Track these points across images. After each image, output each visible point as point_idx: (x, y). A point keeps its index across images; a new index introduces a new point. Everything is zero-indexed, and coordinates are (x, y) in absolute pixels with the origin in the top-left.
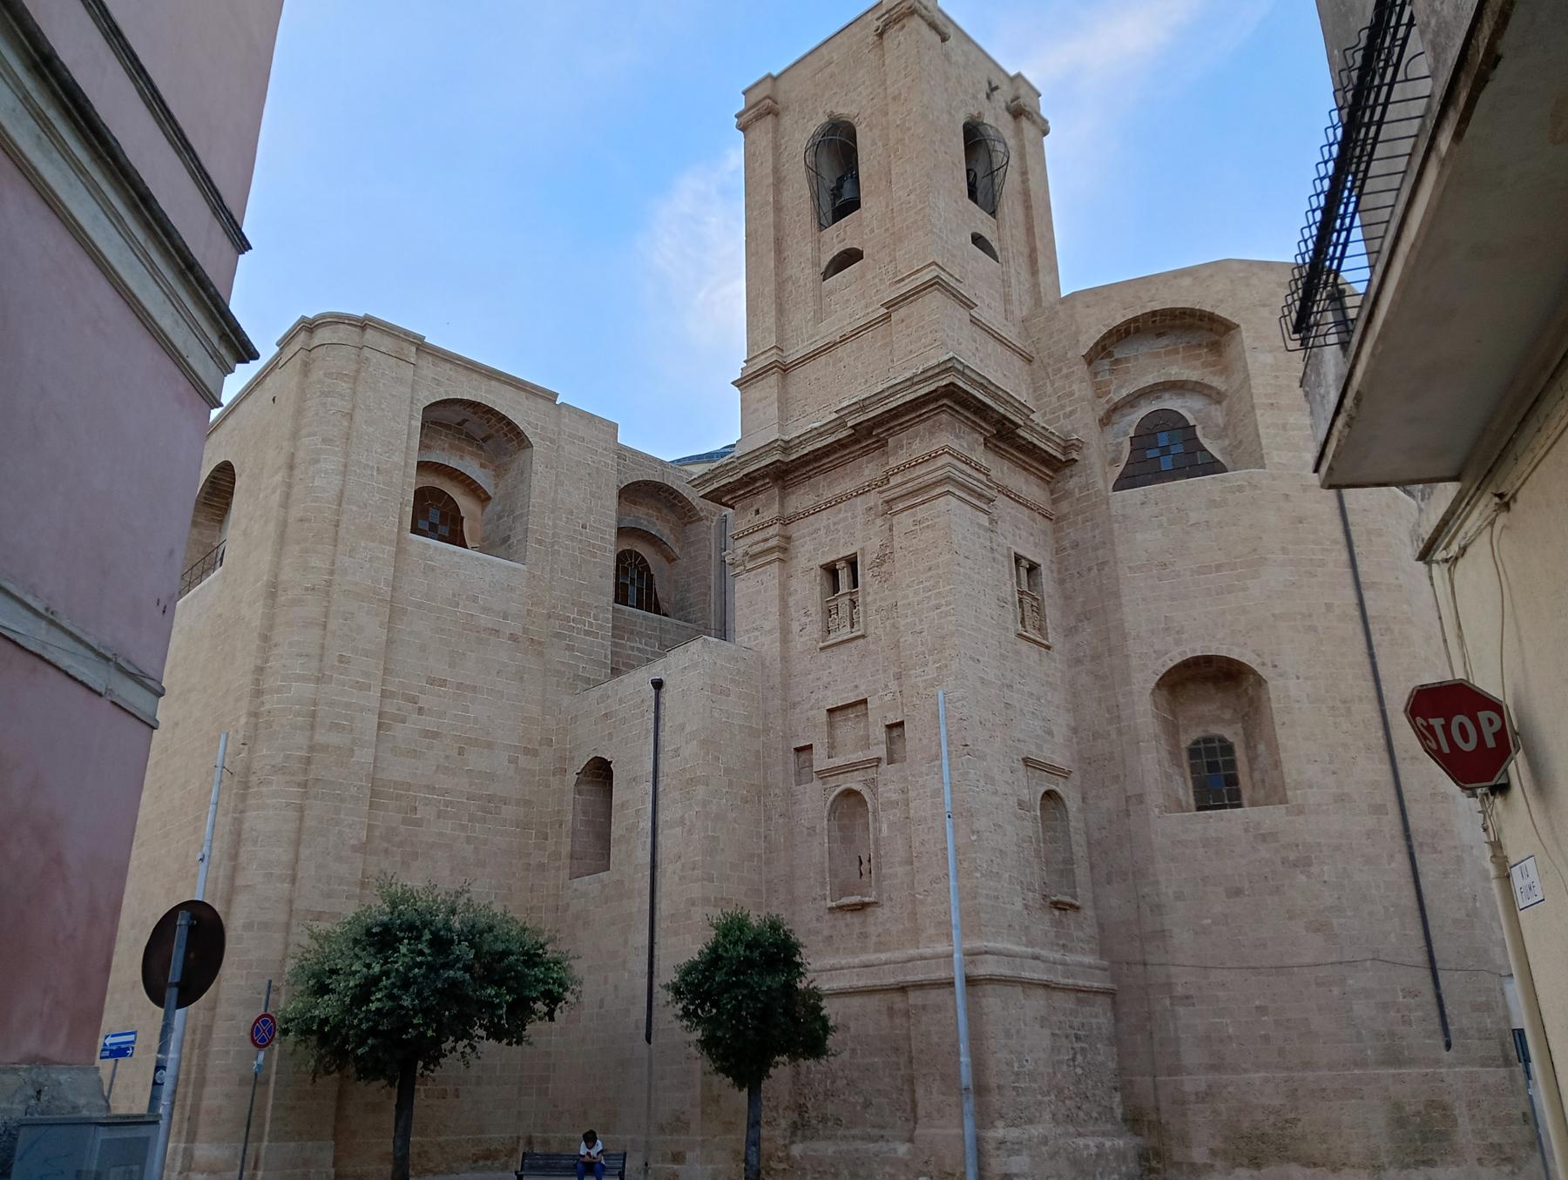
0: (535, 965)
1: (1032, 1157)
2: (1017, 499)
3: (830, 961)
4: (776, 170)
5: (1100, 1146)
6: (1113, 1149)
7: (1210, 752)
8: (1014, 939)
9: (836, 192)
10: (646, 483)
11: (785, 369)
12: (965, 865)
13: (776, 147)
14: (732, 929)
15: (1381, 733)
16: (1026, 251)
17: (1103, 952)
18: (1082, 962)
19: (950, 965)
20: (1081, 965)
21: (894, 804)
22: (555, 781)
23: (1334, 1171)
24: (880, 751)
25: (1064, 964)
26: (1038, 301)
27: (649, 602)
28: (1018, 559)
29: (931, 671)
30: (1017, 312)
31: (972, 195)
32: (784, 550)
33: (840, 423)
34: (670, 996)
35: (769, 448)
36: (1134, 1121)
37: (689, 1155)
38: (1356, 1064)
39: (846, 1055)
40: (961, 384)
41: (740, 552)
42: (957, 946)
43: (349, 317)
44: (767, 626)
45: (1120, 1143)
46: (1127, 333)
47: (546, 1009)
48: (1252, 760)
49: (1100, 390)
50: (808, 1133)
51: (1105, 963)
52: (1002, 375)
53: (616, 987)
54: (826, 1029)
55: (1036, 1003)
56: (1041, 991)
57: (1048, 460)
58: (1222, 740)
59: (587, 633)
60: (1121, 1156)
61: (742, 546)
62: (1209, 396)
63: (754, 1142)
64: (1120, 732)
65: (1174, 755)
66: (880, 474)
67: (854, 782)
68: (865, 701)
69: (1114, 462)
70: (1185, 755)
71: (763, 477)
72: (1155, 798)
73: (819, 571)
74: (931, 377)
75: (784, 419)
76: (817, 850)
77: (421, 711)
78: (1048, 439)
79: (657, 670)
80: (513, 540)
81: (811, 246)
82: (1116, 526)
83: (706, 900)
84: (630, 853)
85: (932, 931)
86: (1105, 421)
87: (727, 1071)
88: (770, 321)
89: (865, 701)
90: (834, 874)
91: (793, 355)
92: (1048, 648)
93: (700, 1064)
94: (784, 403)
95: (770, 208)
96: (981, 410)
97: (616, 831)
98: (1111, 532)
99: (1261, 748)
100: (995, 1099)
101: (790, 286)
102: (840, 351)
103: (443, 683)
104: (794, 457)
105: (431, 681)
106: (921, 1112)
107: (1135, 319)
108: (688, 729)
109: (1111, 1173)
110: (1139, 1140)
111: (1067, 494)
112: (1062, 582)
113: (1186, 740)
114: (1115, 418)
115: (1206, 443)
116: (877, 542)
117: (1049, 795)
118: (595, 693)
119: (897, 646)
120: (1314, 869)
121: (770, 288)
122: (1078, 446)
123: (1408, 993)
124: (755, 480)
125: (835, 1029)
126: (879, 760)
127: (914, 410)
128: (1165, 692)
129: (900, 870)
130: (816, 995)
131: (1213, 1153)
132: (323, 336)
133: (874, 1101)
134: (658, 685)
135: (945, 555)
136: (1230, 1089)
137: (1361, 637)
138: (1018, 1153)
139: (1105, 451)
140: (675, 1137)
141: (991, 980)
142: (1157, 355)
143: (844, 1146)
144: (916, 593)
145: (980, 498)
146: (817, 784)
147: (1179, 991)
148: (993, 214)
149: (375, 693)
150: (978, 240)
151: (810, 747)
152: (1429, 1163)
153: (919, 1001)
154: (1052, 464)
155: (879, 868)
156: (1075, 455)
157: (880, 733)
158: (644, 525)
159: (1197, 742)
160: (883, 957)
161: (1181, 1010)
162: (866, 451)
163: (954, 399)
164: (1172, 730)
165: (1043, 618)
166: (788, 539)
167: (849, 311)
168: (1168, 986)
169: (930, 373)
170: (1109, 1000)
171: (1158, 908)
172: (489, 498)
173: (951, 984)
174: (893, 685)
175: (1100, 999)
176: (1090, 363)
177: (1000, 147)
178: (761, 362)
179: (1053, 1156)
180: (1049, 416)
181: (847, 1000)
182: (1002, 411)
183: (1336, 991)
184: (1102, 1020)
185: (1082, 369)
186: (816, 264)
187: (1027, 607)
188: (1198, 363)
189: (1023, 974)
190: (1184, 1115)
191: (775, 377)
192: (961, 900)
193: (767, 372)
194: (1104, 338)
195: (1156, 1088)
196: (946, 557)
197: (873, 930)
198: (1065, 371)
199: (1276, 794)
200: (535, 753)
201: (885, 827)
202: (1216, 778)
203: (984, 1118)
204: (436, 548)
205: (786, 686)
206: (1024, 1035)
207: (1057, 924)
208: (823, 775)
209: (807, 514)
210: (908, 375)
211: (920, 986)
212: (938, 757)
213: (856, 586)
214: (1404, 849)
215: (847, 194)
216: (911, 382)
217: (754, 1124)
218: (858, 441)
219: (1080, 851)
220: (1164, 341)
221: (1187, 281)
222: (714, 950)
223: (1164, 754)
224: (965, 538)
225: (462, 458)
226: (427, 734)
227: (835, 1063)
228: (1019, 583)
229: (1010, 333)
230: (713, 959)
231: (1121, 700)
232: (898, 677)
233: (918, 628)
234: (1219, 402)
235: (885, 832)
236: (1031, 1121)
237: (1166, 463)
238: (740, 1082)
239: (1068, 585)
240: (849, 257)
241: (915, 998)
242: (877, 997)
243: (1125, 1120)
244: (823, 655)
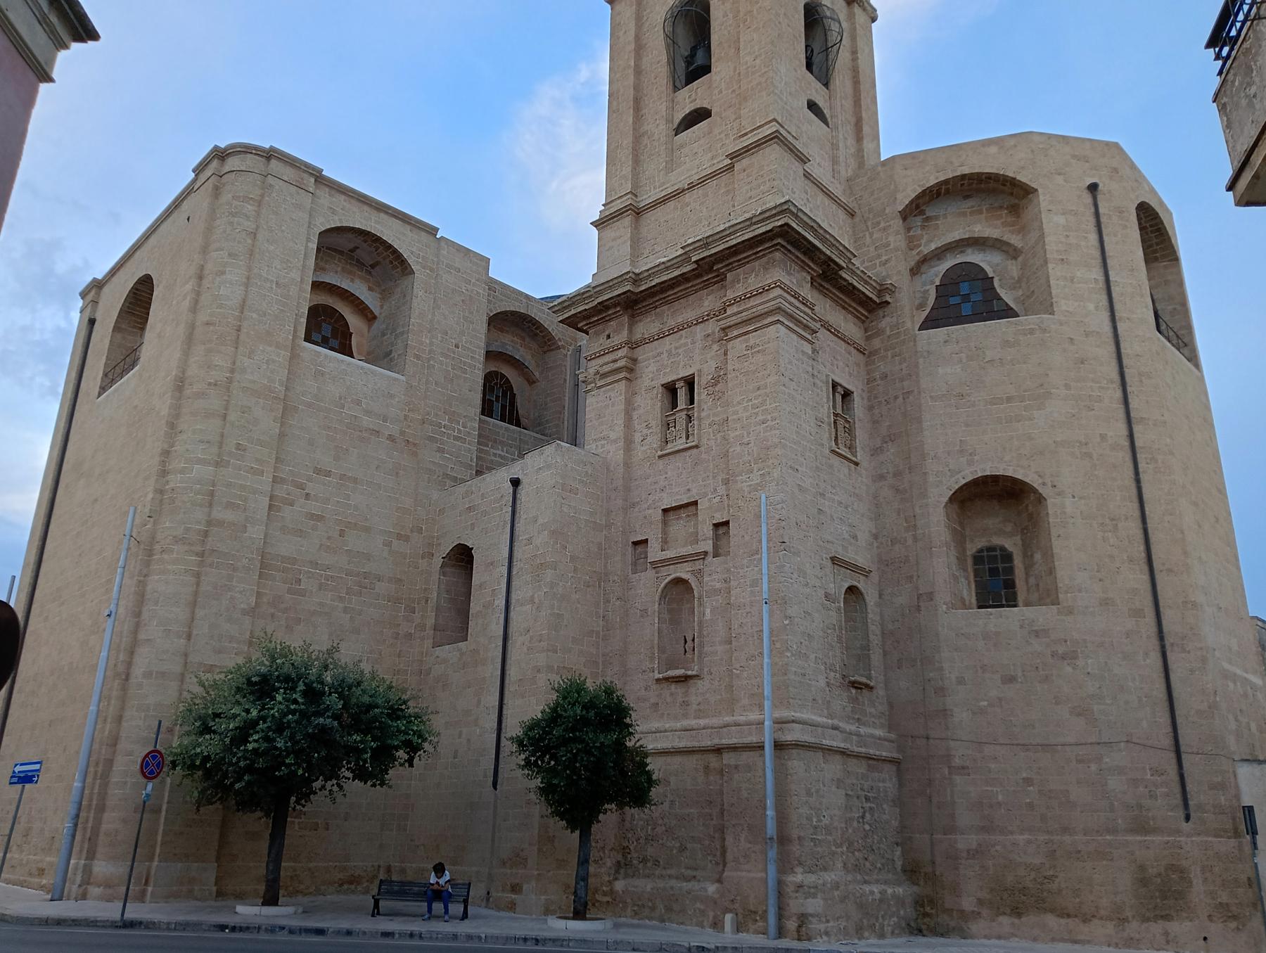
0: (398, 718)
1: (825, 900)
2: (836, 334)
3: (656, 725)
4: (637, 38)
5: (883, 893)
6: (894, 896)
7: (993, 559)
8: (818, 713)
9: (689, 60)
10: (513, 313)
11: (638, 212)
12: (778, 645)
13: (639, 19)
14: (571, 693)
15: (1142, 548)
16: (853, 120)
17: (891, 728)
18: (874, 734)
19: (761, 731)
20: (872, 736)
21: (717, 592)
22: (423, 564)
23: (1084, 921)
24: (708, 546)
25: (858, 735)
26: (861, 164)
27: (511, 416)
28: (835, 385)
29: (756, 479)
30: (843, 173)
31: (809, 66)
32: (631, 370)
33: (685, 258)
34: (514, 748)
35: (621, 279)
36: (912, 872)
37: (525, 887)
38: (1108, 831)
39: (666, 805)
40: (794, 225)
41: (592, 371)
42: (768, 715)
43: (256, 148)
44: (613, 436)
45: (900, 890)
46: (938, 194)
47: (406, 757)
48: (1028, 568)
49: (912, 243)
50: (630, 872)
51: (893, 736)
52: (829, 220)
53: (469, 740)
54: (651, 782)
55: (834, 767)
56: (838, 757)
57: (865, 302)
58: (1003, 549)
59: (456, 438)
60: (900, 902)
61: (594, 366)
62: (1006, 252)
63: (583, 878)
64: (915, 539)
65: (961, 560)
66: (718, 305)
67: (683, 572)
68: (695, 503)
69: (921, 307)
70: (970, 561)
71: (615, 306)
72: (943, 597)
73: (661, 389)
74: (768, 218)
75: (635, 256)
76: (647, 630)
78: (866, 282)
79: (516, 470)
81: (666, 105)
82: (921, 361)
83: (550, 668)
85: (745, 701)
86: (915, 271)
87: (562, 816)
88: (627, 170)
89: (695, 503)
90: (662, 650)
91: (646, 198)
92: (857, 464)
93: (538, 808)
94: (636, 242)
95: (631, 71)
96: (810, 251)
97: (475, 607)
98: (917, 366)
99: (1038, 556)
100: (795, 849)
101: (645, 140)
102: (687, 197)
103: (328, 474)
105: (318, 471)
106: (729, 856)
107: (946, 182)
108: (540, 521)
109: (891, 917)
110: (915, 888)
111: (879, 333)
112: (871, 408)
113: (971, 549)
114: (924, 268)
115: (1002, 293)
116: (713, 364)
117: (852, 590)
118: (461, 489)
119: (726, 455)
120: (1080, 663)
121: (628, 141)
122: (891, 290)
123: (1156, 772)
124: (608, 308)
125: (657, 782)
126: (706, 553)
127: (751, 248)
128: (955, 506)
129: (720, 648)
130: (642, 754)
131: (980, 902)
132: (233, 163)
133: (688, 846)
134: (516, 483)
135: (770, 383)
136: (998, 848)
137: (1130, 464)
138: (814, 896)
139: (913, 297)
140: (514, 871)
141: (797, 745)
142: (964, 214)
143: (661, 884)
144: (745, 409)
145: (806, 329)
146: (650, 573)
147: (957, 762)
148: (826, 85)
149: (267, 478)
150: (812, 106)
151: (646, 541)
152: (1167, 918)
153: (732, 762)
154: (867, 305)
155: (702, 645)
156: (888, 298)
157: (708, 531)
158: (510, 350)
159: (981, 551)
160: (702, 722)
161: (958, 779)
163: (785, 238)
164: (960, 539)
165: (853, 438)
166: (635, 361)
167: (697, 162)
168: (948, 757)
169: (767, 214)
170: (894, 768)
171: (941, 691)
172: (375, 318)
173: (762, 748)
174: (722, 490)
175: (887, 767)
176: (904, 219)
177: (835, 27)
178: (618, 205)
179: (843, 899)
180: (866, 264)
181: (669, 759)
182: (828, 253)
183: (1094, 767)
184: (888, 784)
185: (897, 223)
186: (669, 121)
187: (840, 428)
188: (999, 222)
189: (824, 742)
190: (957, 869)
191: (629, 219)
192: (773, 675)
193: (623, 214)
194: (918, 197)
195: (932, 845)
196: (773, 379)
197: (694, 699)
198: (882, 225)
199: (1049, 596)
200: (407, 539)
201: (708, 611)
202: (996, 582)
203: (785, 865)
204: (326, 356)
205: (627, 489)
206: (822, 794)
207: (854, 700)
208: (656, 565)
209: (652, 340)
210: (747, 216)
211: (734, 748)
212: (757, 552)
213: (692, 402)
214: (1158, 648)
215: (700, 60)
216: (750, 222)
217: (584, 861)
218: (700, 276)
219: (875, 640)
220: (970, 203)
221: (993, 150)
222: (554, 710)
223: (953, 560)
224: (790, 363)
225: (352, 281)
226: (312, 517)
227: (656, 811)
228: (834, 407)
229: (837, 189)
230: (553, 717)
231: (918, 511)
232: (726, 482)
233: (745, 440)
234: (1015, 258)
235: (708, 615)
236: (825, 869)
237: (966, 309)
238: (572, 825)
239: (876, 411)
240: (699, 116)
241: (729, 759)
242: (696, 757)
243: (904, 871)
244: (661, 462)
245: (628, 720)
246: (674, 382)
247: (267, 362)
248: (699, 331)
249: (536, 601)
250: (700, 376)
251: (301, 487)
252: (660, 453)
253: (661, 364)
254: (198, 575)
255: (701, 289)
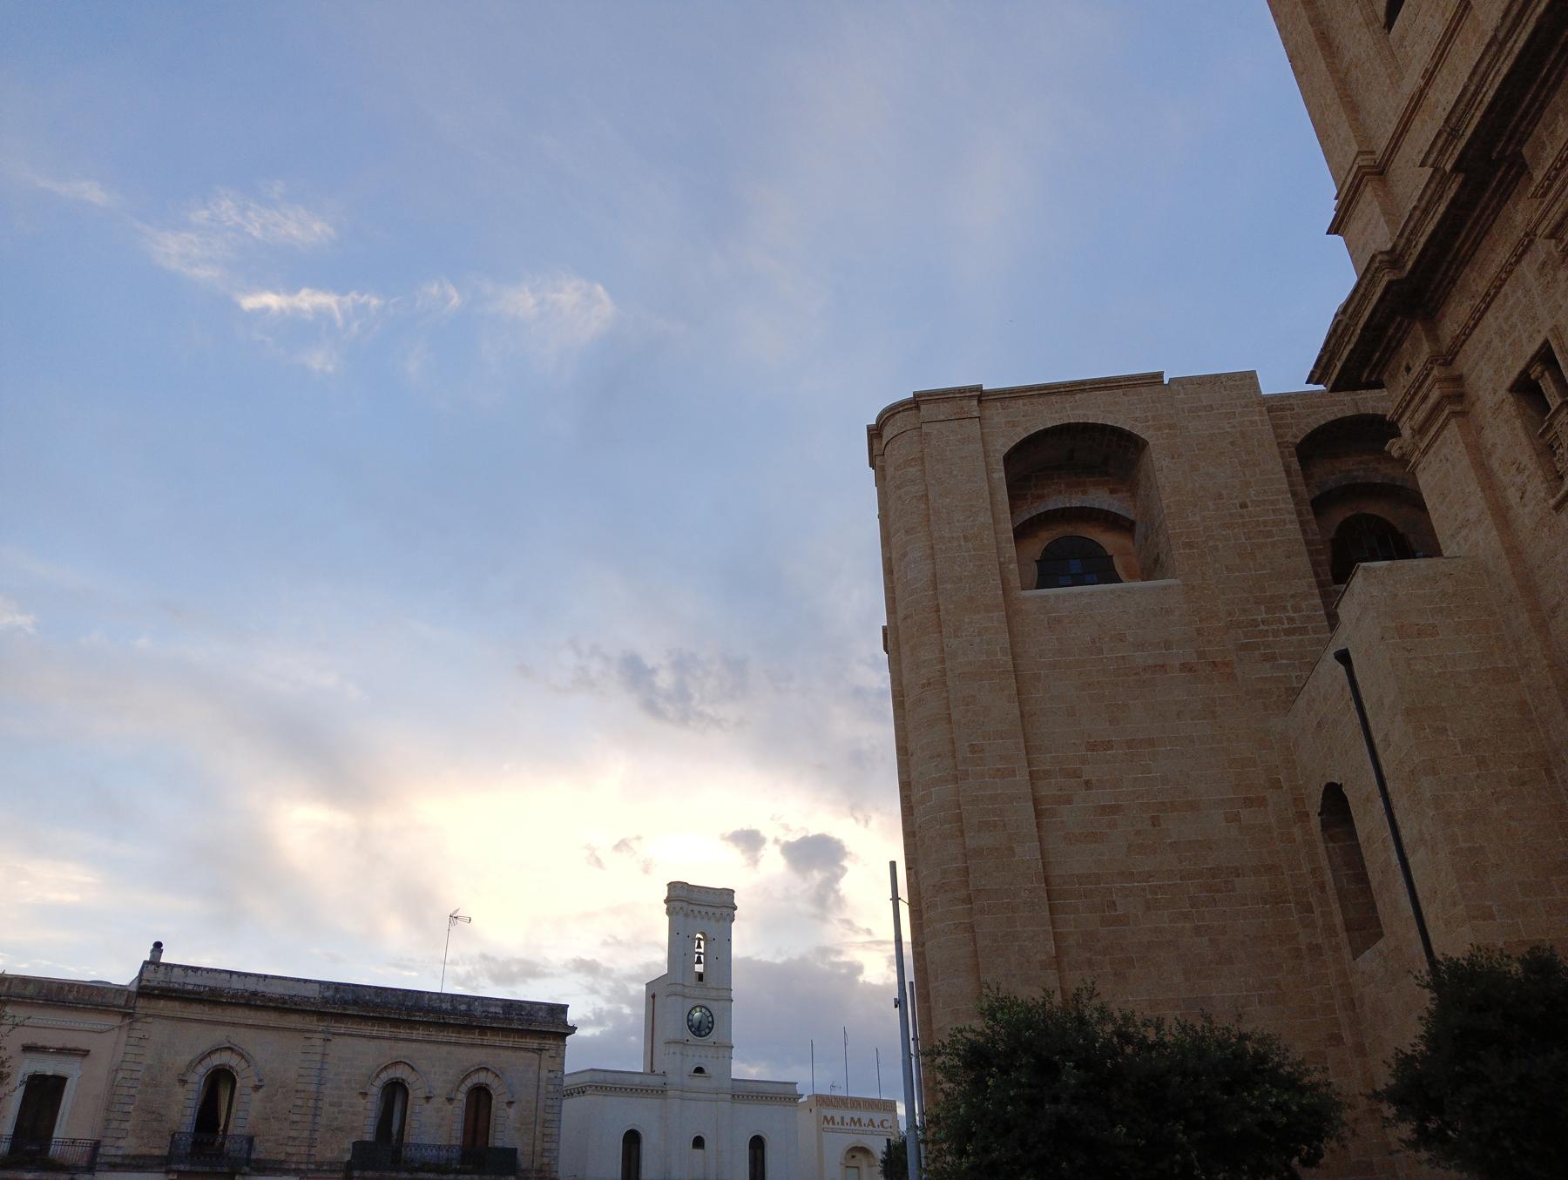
32: (1460, 397)
43: (902, 404)
59: (1288, 632)
77: (1088, 784)
80: (1162, 556)
84: (1392, 903)
103: (1108, 745)
104: (1410, 265)
105: (1092, 747)
132: (888, 433)
134: (1344, 657)
149: (1023, 776)
162: (1505, 193)
166: (1459, 380)
172: (1133, 523)
191: (1369, 189)
200: (1262, 802)
204: (1057, 597)
225: (1084, 492)
226: (1104, 810)
245: (1393, 1081)
246: (1525, 373)
247: (980, 634)
248: (1527, 269)
249: (1427, 837)
250: (1559, 337)
251: (1076, 774)
252: (1552, 502)
253: (1491, 368)
254: (971, 928)
255: (1500, 206)
